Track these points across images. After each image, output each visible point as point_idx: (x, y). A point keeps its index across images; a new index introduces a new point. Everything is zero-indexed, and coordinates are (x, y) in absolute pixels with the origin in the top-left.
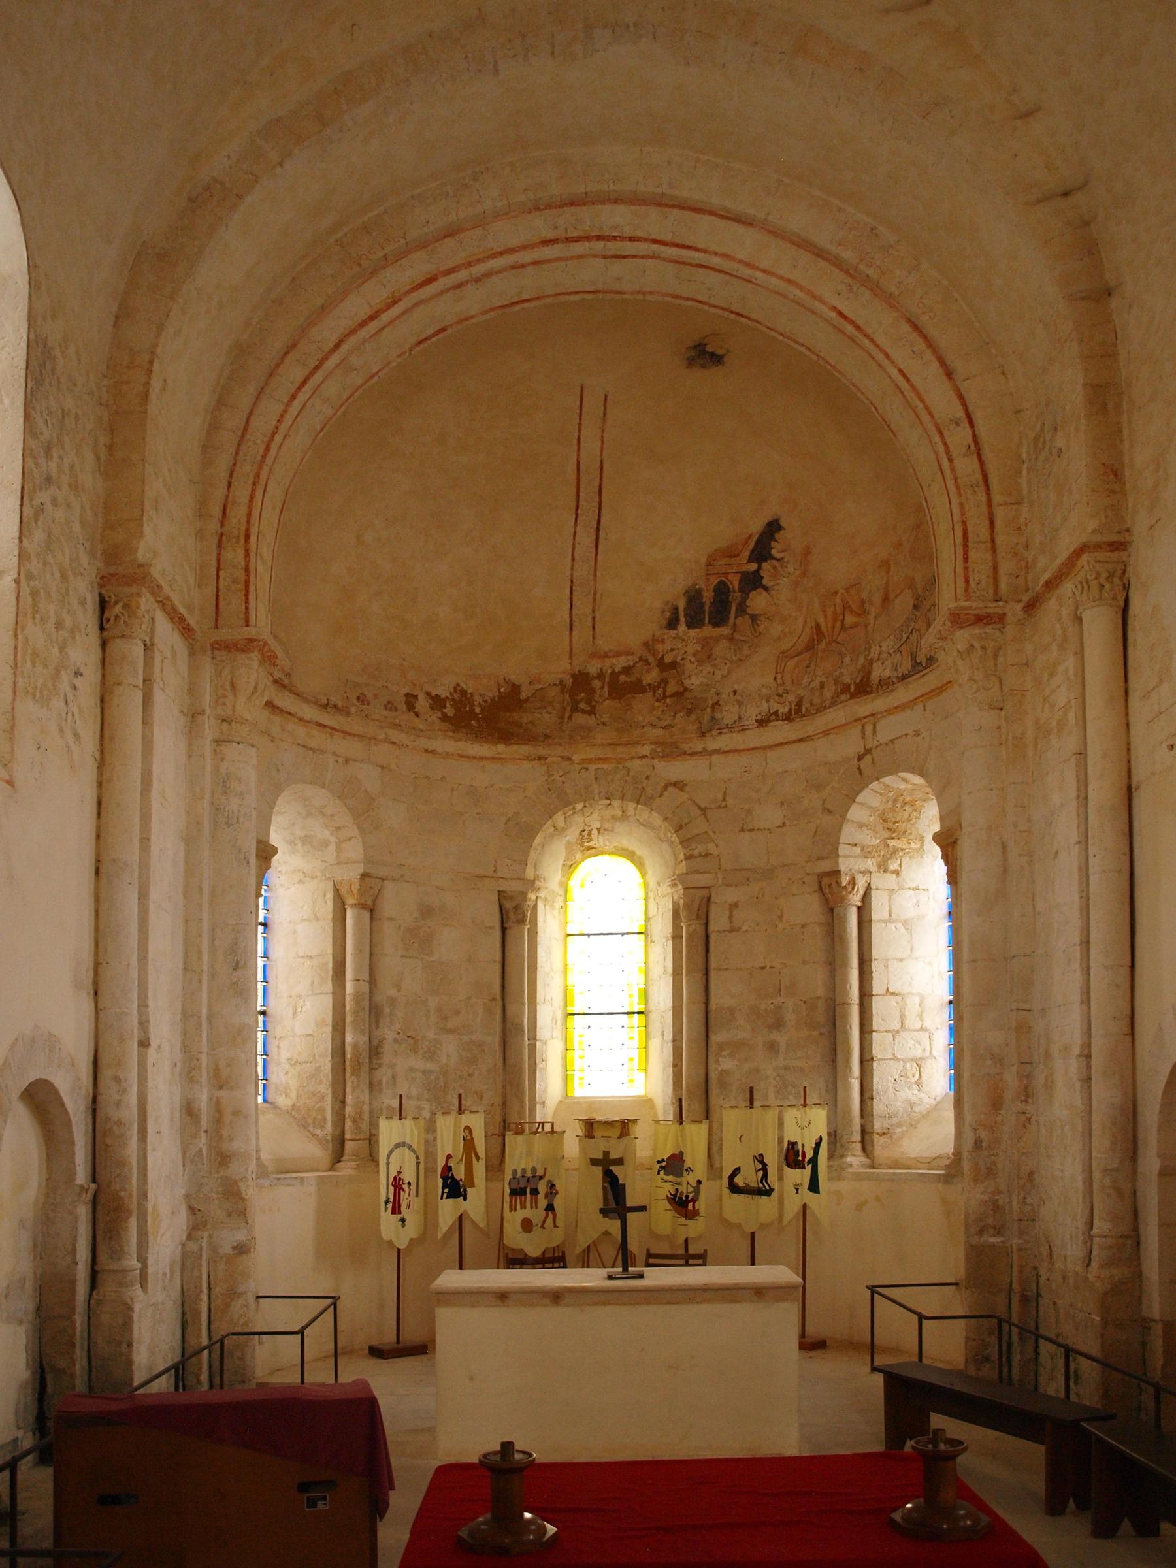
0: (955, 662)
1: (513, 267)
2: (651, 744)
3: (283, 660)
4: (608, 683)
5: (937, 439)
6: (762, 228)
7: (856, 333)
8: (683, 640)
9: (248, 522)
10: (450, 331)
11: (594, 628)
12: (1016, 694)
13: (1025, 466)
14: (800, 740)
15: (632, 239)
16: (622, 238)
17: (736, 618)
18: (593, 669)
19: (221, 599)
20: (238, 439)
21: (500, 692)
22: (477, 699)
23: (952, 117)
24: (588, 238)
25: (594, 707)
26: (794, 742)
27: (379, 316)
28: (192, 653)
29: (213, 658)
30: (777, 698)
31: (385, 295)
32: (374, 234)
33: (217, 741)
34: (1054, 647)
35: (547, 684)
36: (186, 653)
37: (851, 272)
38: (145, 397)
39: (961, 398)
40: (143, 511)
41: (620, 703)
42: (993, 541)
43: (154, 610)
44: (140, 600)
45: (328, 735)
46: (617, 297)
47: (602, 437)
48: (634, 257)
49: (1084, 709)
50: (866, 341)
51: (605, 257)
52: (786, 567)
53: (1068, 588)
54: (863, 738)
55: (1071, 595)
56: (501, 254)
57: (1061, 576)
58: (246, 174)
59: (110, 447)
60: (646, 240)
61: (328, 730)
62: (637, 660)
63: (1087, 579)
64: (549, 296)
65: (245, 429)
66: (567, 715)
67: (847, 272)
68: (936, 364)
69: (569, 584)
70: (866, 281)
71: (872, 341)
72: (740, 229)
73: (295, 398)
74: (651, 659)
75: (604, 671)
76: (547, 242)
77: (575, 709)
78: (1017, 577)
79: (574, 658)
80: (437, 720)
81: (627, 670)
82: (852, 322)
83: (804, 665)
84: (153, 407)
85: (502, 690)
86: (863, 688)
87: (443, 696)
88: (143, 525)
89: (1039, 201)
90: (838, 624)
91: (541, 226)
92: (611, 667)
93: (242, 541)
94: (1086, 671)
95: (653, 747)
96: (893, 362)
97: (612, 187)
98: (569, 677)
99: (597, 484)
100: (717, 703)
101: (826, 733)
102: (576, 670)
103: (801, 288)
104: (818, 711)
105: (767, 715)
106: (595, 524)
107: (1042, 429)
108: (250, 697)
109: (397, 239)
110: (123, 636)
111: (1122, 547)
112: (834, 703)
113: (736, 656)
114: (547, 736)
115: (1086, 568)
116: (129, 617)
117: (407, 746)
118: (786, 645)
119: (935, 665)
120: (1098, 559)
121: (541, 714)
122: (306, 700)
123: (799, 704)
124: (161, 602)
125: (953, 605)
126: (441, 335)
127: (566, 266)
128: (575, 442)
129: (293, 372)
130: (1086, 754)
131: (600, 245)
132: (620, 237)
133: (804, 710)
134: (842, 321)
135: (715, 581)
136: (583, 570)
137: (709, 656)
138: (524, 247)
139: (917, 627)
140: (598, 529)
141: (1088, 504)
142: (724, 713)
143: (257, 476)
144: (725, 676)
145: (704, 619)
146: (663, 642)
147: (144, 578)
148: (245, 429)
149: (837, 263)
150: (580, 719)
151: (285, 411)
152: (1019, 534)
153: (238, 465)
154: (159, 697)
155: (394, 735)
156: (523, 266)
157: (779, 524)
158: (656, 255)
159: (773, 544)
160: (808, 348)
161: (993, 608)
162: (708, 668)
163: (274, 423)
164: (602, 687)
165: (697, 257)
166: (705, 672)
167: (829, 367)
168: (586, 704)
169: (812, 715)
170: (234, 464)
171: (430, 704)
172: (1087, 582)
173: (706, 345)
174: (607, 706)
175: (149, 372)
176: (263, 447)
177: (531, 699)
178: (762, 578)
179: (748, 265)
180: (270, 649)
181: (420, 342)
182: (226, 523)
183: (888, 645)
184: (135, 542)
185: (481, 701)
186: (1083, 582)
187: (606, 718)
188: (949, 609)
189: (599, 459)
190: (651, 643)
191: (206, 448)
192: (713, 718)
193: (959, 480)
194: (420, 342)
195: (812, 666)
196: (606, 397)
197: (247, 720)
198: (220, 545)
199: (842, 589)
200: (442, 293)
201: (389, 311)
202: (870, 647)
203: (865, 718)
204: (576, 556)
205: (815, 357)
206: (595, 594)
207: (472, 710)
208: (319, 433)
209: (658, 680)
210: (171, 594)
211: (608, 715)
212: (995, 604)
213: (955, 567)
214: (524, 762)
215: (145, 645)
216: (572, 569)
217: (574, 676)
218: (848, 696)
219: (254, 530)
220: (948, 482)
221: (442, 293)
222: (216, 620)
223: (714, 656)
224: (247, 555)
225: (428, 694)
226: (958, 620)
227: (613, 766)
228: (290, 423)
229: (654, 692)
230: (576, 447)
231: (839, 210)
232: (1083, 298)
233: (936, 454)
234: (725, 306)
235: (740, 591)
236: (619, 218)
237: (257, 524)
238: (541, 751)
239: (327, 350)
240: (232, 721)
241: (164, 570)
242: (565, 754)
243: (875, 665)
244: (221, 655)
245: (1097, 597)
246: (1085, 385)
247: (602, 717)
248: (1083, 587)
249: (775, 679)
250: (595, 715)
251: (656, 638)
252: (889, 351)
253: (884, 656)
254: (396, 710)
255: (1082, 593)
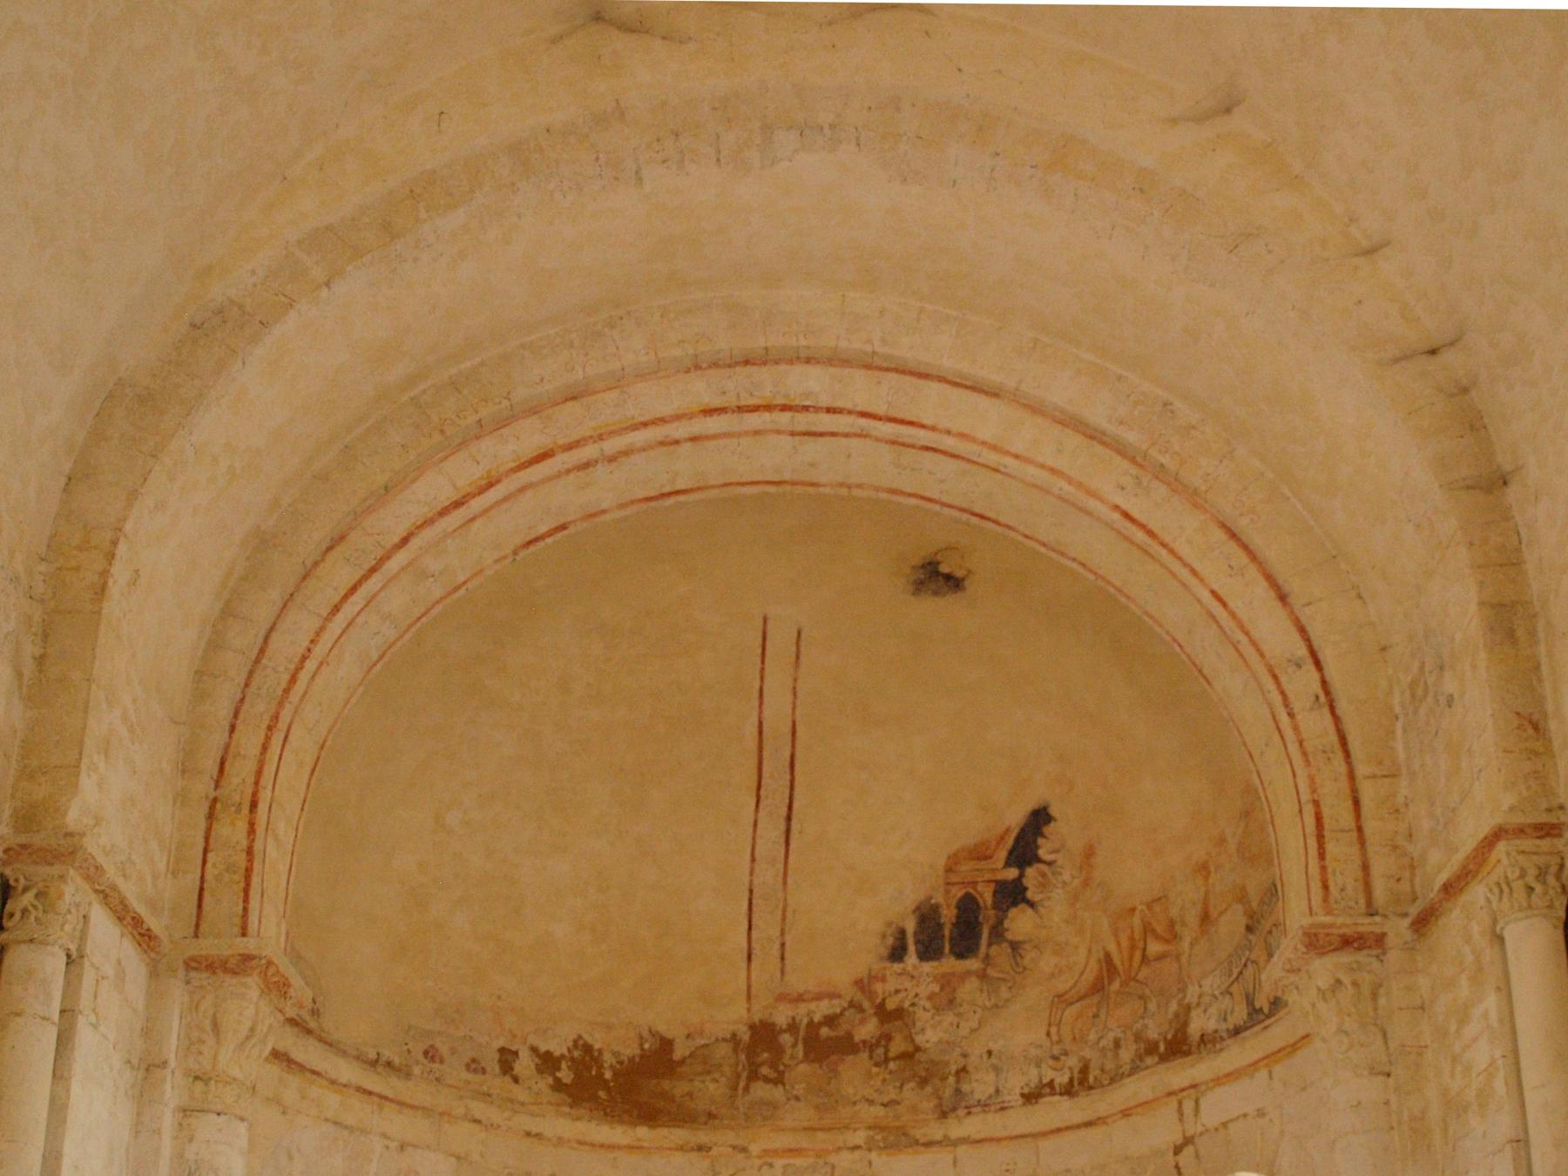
0: (1313, 1005)
1: (662, 443)
2: (870, 1128)
3: (300, 989)
4: (804, 1039)
5: (1270, 685)
6: (1013, 400)
7: (1148, 540)
8: (913, 977)
9: (257, 783)
10: (572, 530)
11: (783, 958)
12: (1410, 1053)
13: (1399, 725)
14: (1089, 1124)
15: (829, 410)
16: (817, 409)
17: (990, 945)
18: (781, 1017)
19: (206, 894)
20: (249, 665)
21: (642, 1049)
22: (608, 1059)
23: (1269, 252)
24: (769, 408)
25: (781, 1073)
26: (1078, 1127)
27: (467, 502)
28: (154, 974)
29: (188, 982)
30: (1051, 1062)
31: (479, 475)
32: (465, 392)
33: (185, 1111)
34: (1464, 981)
35: (713, 1039)
36: (143, 971)
37: (1138, 459)
38: (101, 591)
39: (1302, 630)
40: (81, 754)
41: (821, 1067)
42: (1360, 829)
43: (90, 904)
44: (63, 886)
45: (375, 1107)
46: (811, 490)
47: (794, 688)
48: (833, 434)
49: (1518, 1071)
50: (1164, 552)
51: (793, 434)
52: (1060, 874)
53: (1478, 893)
54: (1181, 1120)
55: (1482, 902)
56: (645, 424)
57: (1467, 875)
58: (277, 295)
59: (41, 660)
60: (850, 412)
61: (376, 1099)
62: (846, 1005)
63: (1506, 878)
64: (713, 487)
65: (262, 651)
66: (742, 1084)
67: (1133, 460)
68: (1264, 584)
69: (747, 894)
70: (1160, 472)
71: (1172, 552)
72: (983, 402)
73: (338, 611)
74: (866, 1005)
75: (797, 1021)
76: (709, 412)
77: (754, 1076)
78: (1399, 880)
79: (753, 1001)
80: (546, 1090)
81: (830, 1020)
82: (1142, 526)
83: (1091, 1014)
84: (113, 605)
85: (647, 1046)
86: (1177, 1047)
87: (557, 1053)
88: (78, 775)
89: (1396, 360)
90: (1138, 955)
91: (702, 390)
92: (808, 1015)
93: (246, 810)
94: (1517, 1014)
95: (871, 1133)
96: (1202, 580)
97: (803, 342)
98: (745, 1028)
99: (787, 754)
100: (964, 1069)
101: (1126, 1113)
102: (756, 1018)
103: (1070, 481)
104: (1112, 1080)
105: (1036, 1087)
106: (784, 810)
107: (1422, 668)
108: (242, 1044)
109: (497, 400)
110: (31, 941)
111: (1556, 832)
112: (1134, 1070)
113: (990, 1000)
114: (711, 1116)
115: (1505, 861)
116: (44, 911)
117: (499, 1126)
118: (1062, 985)
119: (1285, 1011)
120: (1521, 848)
121: (703, 1082)
122: (344, 1053)
123: (1085, 1070)
124: (103, 891)
125: (1307, 921)
126: (559, 536)
127: (739, 445)
128: (756, 695)
129: (338, 574)
130: (1527, 1143)
131: (784, 418)
132: (814, 407)
133: (1091, 1079)
134: (1128, 524)
135: (958, 893)
136: (768, 876)
137: (951, 1001)
138: (678, 417)
139: (1253, 957)
140: (789, 818)
141: (1500, 770)
142: (975, 1085)
143: (276, 717)
144: (976, 1030)
145: (943, 947)
146: (883, 979)
147: (72, 853)
148: (262, 651)
149: (1120, 449)
150: (761, 1090)
151: (322, 629)
152: (1397, 819)
153: (247, 700)
154: (85, 1037)
155: (479, 1109)
156: (677, 442)
157: (1048, 814)
158: (900, 936)
159: (1040, 841)
160: (1083, 565)
161: (1366, 925)
162: (949, 1018)
163: (306, 644)
164: (795, 1045)
165: (923, 436)
166: (945, 1024)
167: (1112, 590)
168: (770, 1068)
169: (1103, 1086)
170: (242, 700)
171: (537, 1065)
172: (1508, 884)
173: (938, 563)
174: (802, 1072)
175: (111, 556)
176: (286, 677)
177: (688, 1061)
178: (1026, 889)
179: (994, 448)
180: (278, 972)
181: (530, 543)
182: (223, 783)
183: (1213, 983)
184: (64, 799)
185: (614, 1061)
186: (1501, 882)
187: (799, 1089)
188: (1302, 927)
189: (790, 719)
190: (866, 981)
191: (203, 674)
192: (958, 1091)
193: (1305, 744)
194: (530, 543)
195: (1103, 1016)
196: (799, 633)
197: (235, 1079)
198: (211, 816)
199: (1141, 904)
200: (558, 475)
201: (482, 496)
202: (1187, 987)
203: (1183, 1090)
204: (757, 855)
205: (1092, 577)
206: (784, 911)
207: (600, 1075)
208: (375, 665)
209: (878, 1033)
210: (120, 882)
211: (804, 1085)
212: (1368, 920)
213: (1307, 867)
214: (676, 1153)
215: (69, 956)
216: (751, 873)
217: (752, 1027)
218: (1156, 1059)
219: (265, 796)
220: (1289, 745)
221: (558, 475)
222: (197, 926)
223: (958, 1000)
224: (252, 831)
225: (534, 1050)
226: (1315, 942)
227: (811, 1160)
228: (330, 645)
229: (871, 1051)
230: (756, 703)
231: (1120, 378)
232: (1468, 487)
233: (1271, 706)
234: (964, 505)
235: (994, 908)
236: (812, 383)
237: (270, 787)
238: (703, 1137)
239: (388, 546)
240: (210, 1079)
241: (113, 846)
242: (740, 1142)
243: (1194, 1014)
244: (200, 978)
245: (1525, 905)
246: (1482, 604)
247: (793, 1088)
248: (1501, 891)
249: (1048, 1034)
250: (784, 1084)
251: (873, 973)
252: (1197, 566)
253: (1207, 999)
254: (484, 1071)
255: (1501, 898)
